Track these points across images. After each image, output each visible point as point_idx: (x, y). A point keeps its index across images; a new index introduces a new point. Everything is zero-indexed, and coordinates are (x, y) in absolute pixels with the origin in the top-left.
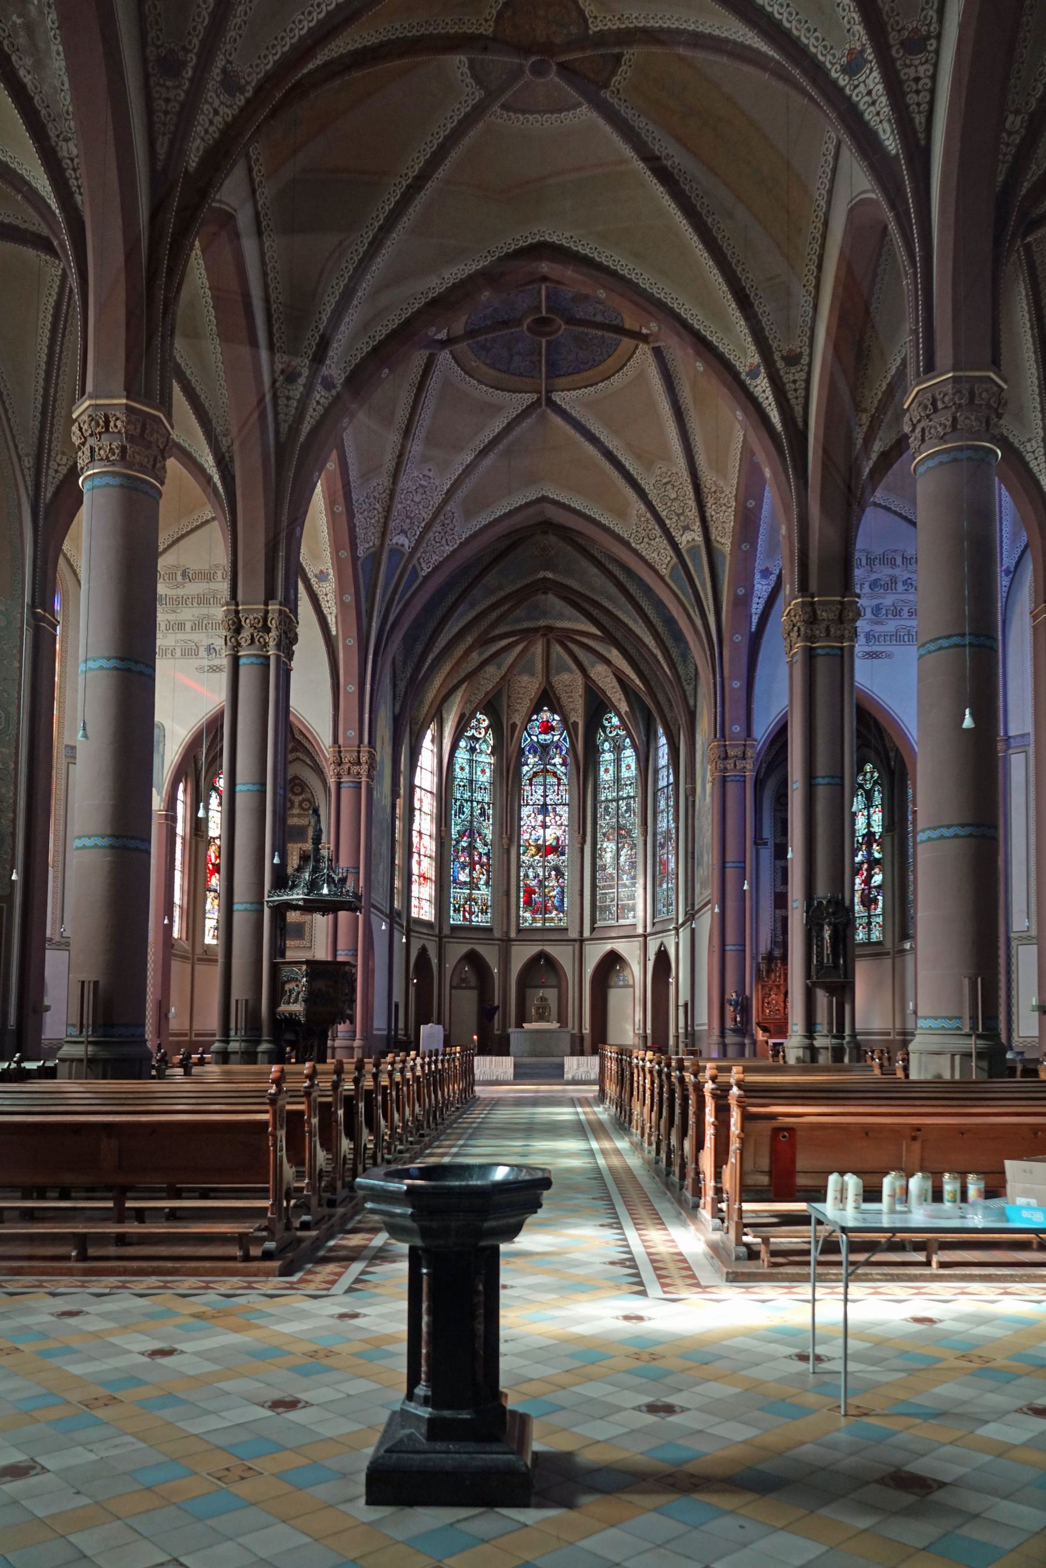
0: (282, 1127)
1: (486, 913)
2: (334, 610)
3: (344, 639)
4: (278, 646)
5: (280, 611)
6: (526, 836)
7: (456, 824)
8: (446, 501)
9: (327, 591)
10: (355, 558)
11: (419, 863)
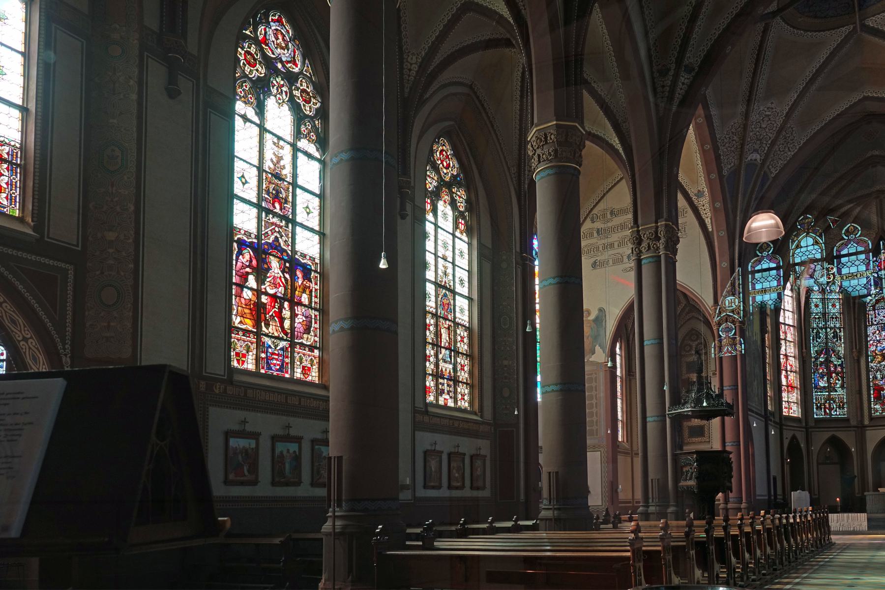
0: (639, 561)
1: (843, 408)
2: (709, 214)
3: (718, 232)
4: (666, 248)
5: (666, 225)
6: (873, 348)
7: (814, 347)
8: (785, 122)
9: (705, 205)
10: (721, 176)
11: (787, 377)
